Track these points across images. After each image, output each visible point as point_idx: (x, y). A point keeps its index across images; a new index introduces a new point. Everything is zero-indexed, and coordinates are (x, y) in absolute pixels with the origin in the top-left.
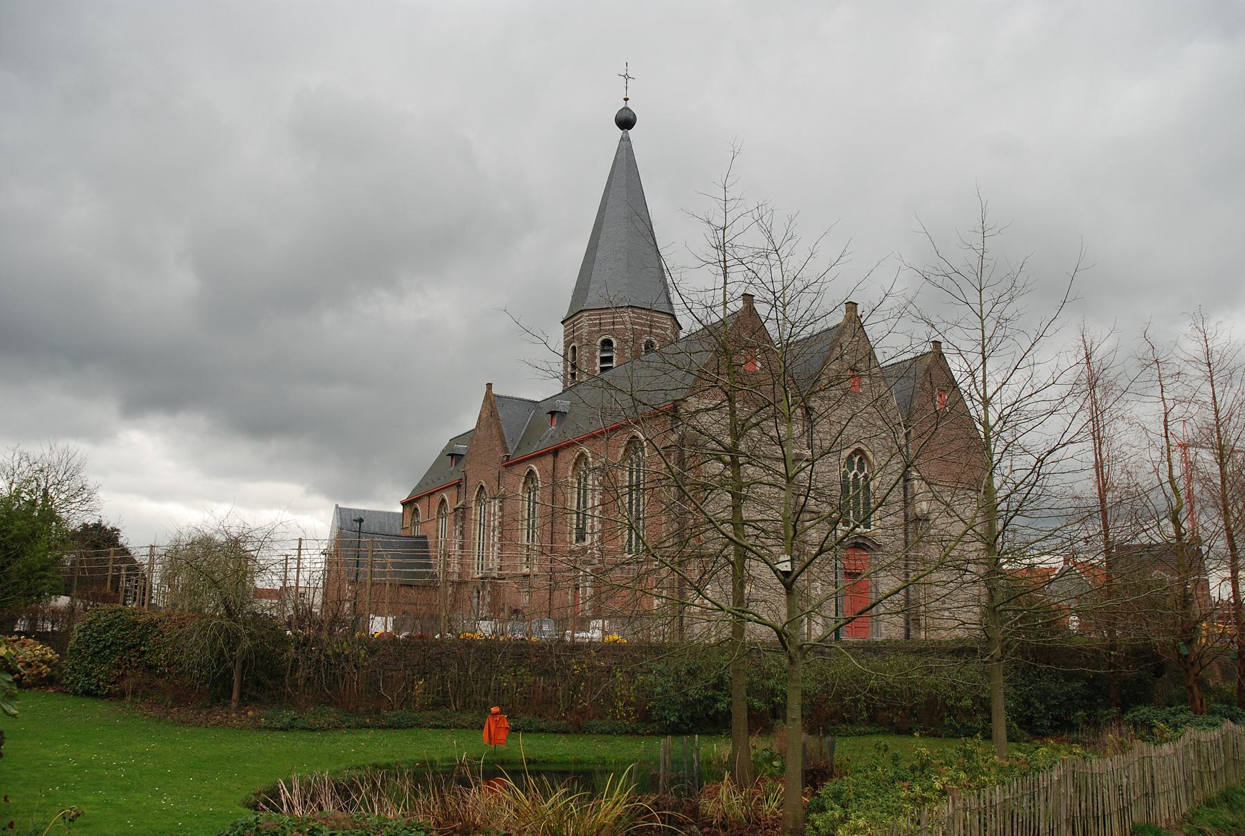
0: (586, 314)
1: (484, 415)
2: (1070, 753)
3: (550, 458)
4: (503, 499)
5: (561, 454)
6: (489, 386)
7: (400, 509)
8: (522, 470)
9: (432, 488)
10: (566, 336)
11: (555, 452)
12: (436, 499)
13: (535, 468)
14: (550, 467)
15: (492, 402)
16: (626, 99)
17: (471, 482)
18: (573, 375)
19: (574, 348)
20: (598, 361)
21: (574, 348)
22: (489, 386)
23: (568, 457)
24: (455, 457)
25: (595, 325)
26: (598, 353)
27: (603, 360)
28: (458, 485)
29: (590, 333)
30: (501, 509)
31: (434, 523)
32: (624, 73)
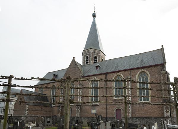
0: (91, 49)
6: (74, 58)
16: (94, 11)
21: (87, 57)
22: (74, 58)
25: (93, 52)
27: (95, 60)
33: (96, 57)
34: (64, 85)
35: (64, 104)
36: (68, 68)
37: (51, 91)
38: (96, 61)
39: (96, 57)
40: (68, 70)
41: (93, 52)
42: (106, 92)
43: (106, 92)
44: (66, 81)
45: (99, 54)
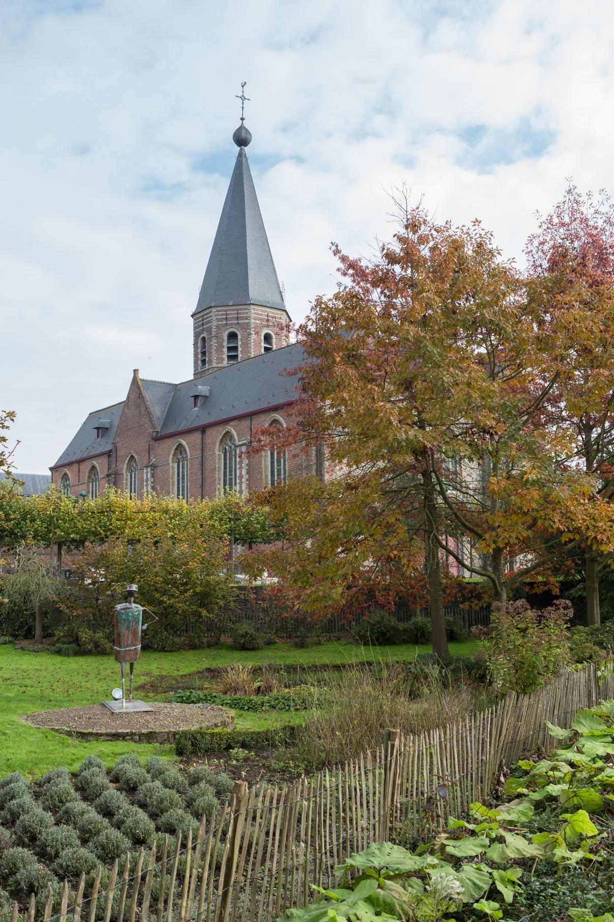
0: (214, 310)
1: (132, 397)
2: (148, 674)
3: (197, 436)
4: (154, 467)
5: (209, 432)
6: (136, 371)
7: (49, 473)
8: (172, 444)
9: (78, 456)
10: (195, 328)
11: (203, 429)
12: (86, 467)
13: (184, 443)
14: (199, 441)
15: (136, 385)
16: (242, 119)
17: (121, 453)
18: (204, 362)
19: (204, 339)
20: (225, 350)
21: (204, 339)
22: (136, 371)
23: (216, 435)
24: (102, 431)
25: (221, 320)
26: (225, 344)
27: (229, 349)
28: (109, 454)
29: (218, 327)
30: (153, 476)
31: (85, 486)
32: (240, 94)
33: (233, 336)
34: (134, 550)
35: (66, 572)
36: (124, 399)
37: (88, 485)
38: (235, 349)
39: (233, 336)
40: (126, 404)
41: (221, 320)
42: (202, 486)
43: (202, 486)
44: (180, 457)
45: (246, 318)
